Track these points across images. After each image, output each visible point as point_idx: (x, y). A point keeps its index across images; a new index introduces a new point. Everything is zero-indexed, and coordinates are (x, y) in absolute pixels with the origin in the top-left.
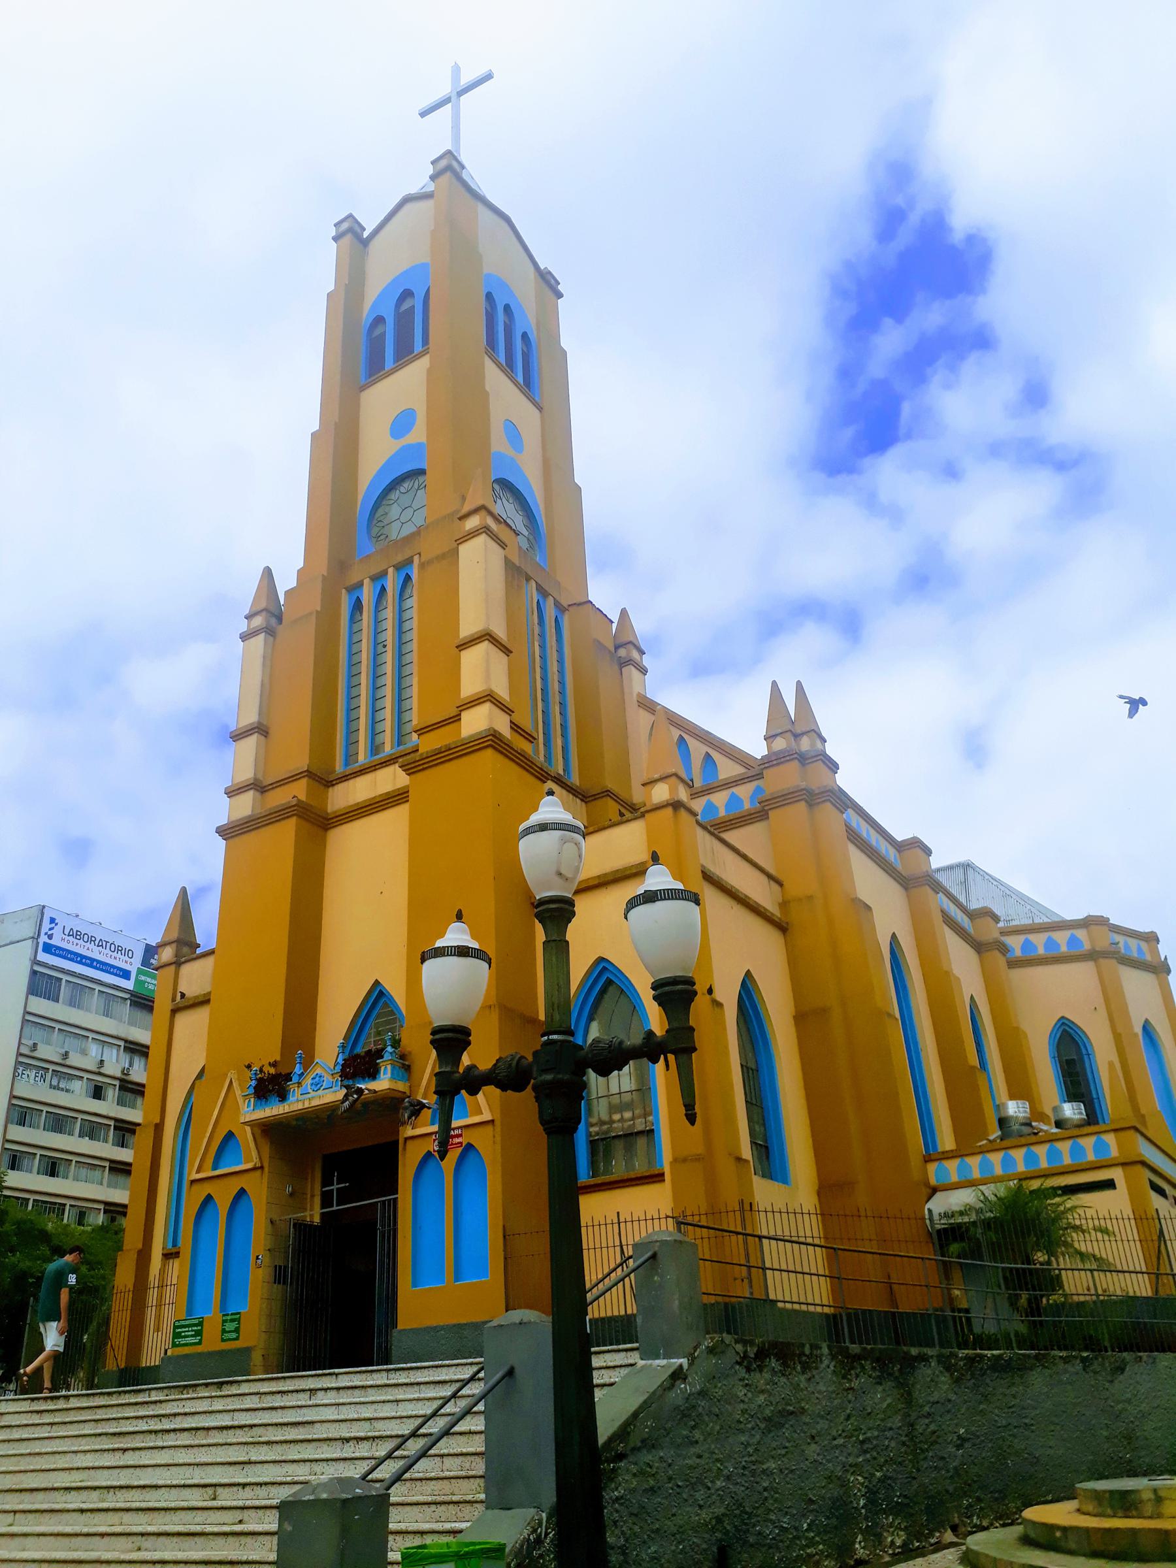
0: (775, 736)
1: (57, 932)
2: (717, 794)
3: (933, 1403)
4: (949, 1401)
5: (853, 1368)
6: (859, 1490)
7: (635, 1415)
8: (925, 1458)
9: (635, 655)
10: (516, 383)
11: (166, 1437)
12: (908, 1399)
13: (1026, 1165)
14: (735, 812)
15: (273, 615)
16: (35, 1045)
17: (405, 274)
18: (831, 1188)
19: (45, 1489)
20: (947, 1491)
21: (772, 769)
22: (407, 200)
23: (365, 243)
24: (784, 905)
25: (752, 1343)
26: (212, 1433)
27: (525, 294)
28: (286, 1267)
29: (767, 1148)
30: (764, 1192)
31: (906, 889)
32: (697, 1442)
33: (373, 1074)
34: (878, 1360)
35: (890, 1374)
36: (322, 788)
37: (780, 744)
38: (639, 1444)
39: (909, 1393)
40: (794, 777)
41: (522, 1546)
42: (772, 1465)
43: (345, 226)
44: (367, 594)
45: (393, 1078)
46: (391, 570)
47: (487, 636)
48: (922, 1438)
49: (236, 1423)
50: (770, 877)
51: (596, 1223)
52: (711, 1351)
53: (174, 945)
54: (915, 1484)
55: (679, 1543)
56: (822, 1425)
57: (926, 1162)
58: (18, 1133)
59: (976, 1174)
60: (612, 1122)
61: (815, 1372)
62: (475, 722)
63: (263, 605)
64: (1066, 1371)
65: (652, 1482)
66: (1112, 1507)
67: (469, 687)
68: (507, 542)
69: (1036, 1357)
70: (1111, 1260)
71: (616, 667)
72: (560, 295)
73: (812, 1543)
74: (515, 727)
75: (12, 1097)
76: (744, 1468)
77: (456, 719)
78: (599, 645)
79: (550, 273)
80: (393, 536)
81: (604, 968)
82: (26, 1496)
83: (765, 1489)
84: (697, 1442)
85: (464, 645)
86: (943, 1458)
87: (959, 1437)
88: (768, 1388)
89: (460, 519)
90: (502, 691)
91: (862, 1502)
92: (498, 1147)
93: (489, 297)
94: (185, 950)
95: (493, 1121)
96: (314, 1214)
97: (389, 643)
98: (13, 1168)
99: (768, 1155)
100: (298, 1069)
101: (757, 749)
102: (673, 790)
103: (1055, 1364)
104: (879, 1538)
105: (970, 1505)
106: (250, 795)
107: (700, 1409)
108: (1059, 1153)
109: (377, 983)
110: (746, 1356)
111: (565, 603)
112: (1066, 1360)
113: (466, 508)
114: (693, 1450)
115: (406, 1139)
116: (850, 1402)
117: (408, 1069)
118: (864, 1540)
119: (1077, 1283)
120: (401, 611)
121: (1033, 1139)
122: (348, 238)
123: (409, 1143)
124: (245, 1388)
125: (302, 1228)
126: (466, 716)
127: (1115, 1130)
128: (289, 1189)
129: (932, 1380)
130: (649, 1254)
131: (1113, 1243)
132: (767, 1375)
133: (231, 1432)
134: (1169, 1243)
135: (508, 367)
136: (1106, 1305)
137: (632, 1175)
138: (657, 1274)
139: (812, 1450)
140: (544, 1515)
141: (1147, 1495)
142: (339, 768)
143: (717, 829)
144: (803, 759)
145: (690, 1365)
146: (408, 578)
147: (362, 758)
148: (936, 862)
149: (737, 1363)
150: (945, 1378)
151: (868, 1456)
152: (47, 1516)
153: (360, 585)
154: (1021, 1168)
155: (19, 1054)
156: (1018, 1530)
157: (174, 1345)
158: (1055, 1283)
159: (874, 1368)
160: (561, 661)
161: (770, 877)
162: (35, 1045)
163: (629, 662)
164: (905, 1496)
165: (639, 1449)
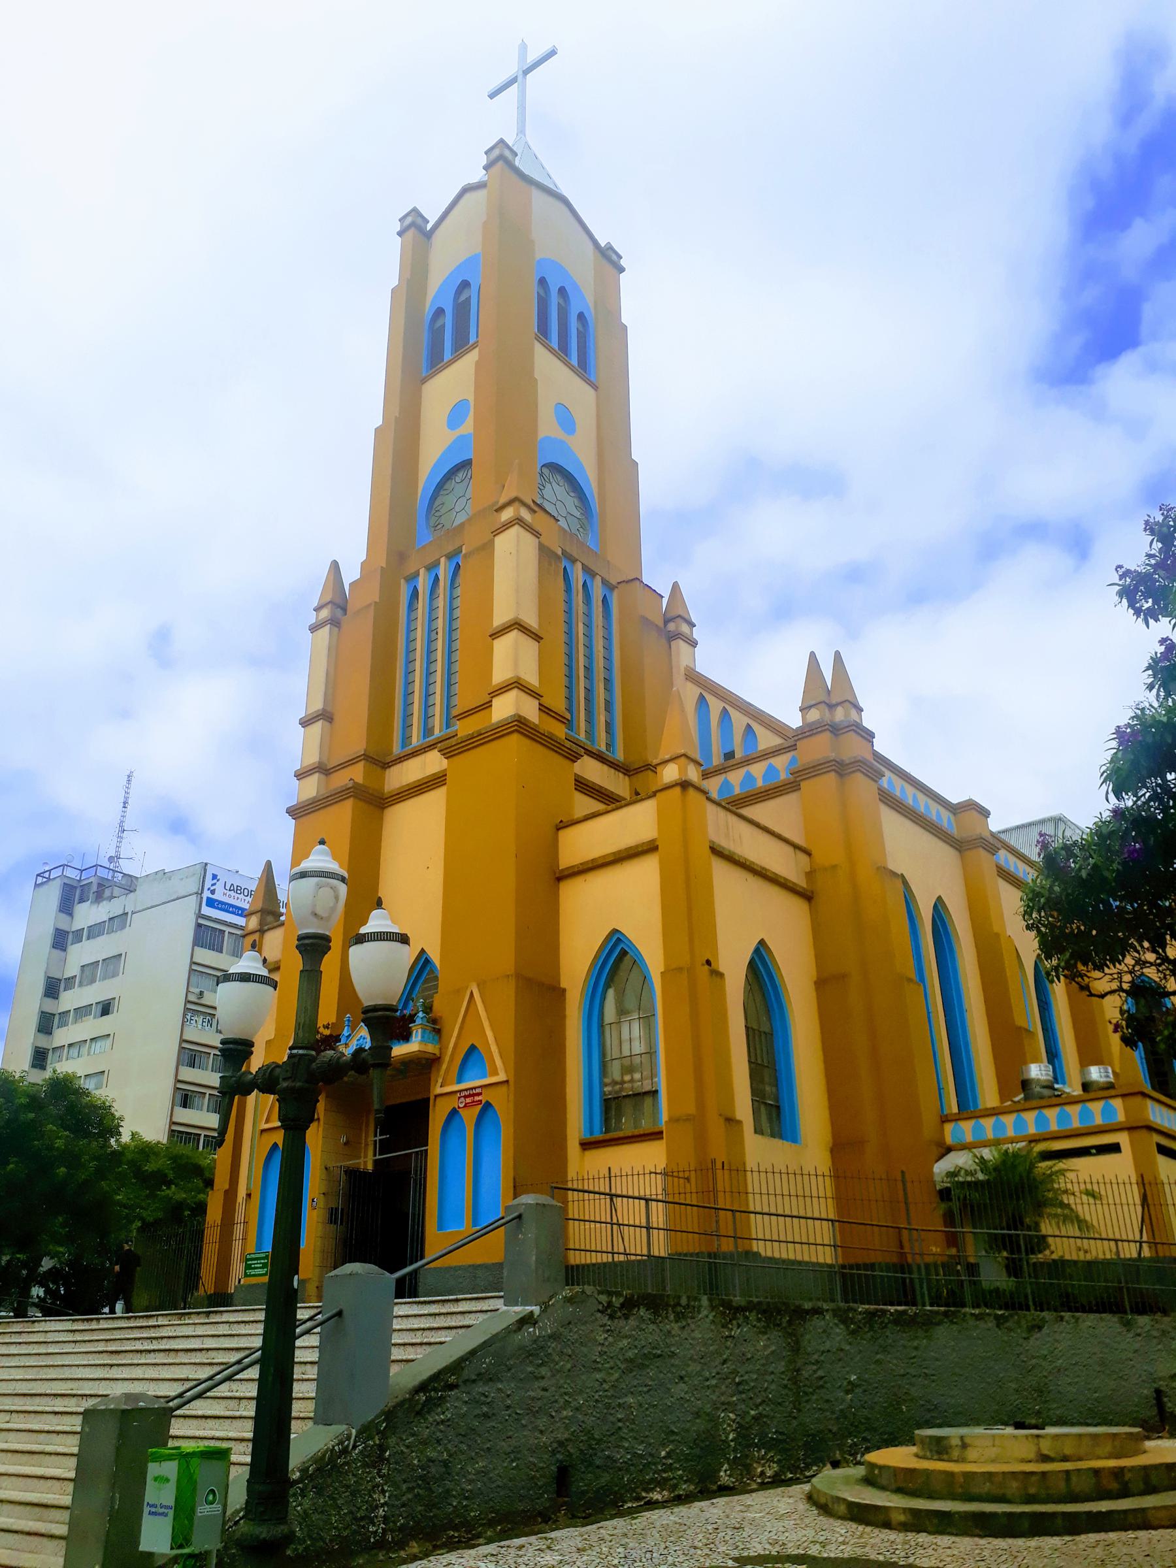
0: (810, 707)
1: (219, 888)
2: (755, 765)
3: (823, 1352)
4: (842, 1350)
5: (734, 1319)
6: (729, 1425)
7: (473, 1353)
8: (807, 1401)
9: (685, 628)
10: (567, 364)
11: (148, 1355)
12: (796, 1349)
13: (1059, 1123)
14: (773, 782)
15: (339, 607)
16: (201, 993)
17: (458, 268)
18: (843, 1146)
19: (40, 1395)
20: (830, 1431)
21: (805, 740)
22: (466, 190)
23: (429, 235)
24: (810, 875)
25: (618, 1294)
26: (180, 1354)
27: (582, 272)
28: (337, 1209)
29: (778, 1107)
30: (759, 1150)
31: (960, 851)
32: (543, 1378)
33: (406, 1037)
34: (764, 1312)
35: (778, 1325)
36: (379, 769)
37: (814, 715)
38: (474, 1377)
39: (797, 1342)
40: (830, 746)
41: (324, 1455)
42: (630, 1400)
43: (409, 220)
44: (423, 583)
45: (423, 1041)
46: (443, 560)
47: (517, 625)
48: (808, 1383)
49: (205, 1346)
50: (796, 847)
51: (635, 1172)
52: (569, 1300)
53: (259, 915)
54: (795, 1423)
55: (513, 1461)
56: (694, 1367)
57: (943, 1122)
58: (188, 1074)
59: (969, 1138)
60: (623, 1082)
61: (689, 1321)
62: (503, 708)
63: (328, 598)
64: (976, 1327)
65: (485, 1409)
66: (931, 1451)
67: (500, 675)
68: (540, 531)
69: (946, 1314)
70: (1095, 1223)
71: (664, 641)
72: (622, 270)
73: (670, 1468)
74: (544, 709)
75: (183, 1041)
76: (597, 1401)
77: (487, 705)
78: (646, 621)
79: (611, 248)
80: (448, 526)
81: (619, 940)
82: (28, 1400)
83: (619, 1420)
84: (543, 1378)
85: (495, 635)
86: (828, 1401)
87: (850, 1382)
88: (640, 1332)
89: (496, 511)
90: (531, 677)
91: (731, 1437)
92: (511, 1105)
93: (542, 282)
94: (270, 918)
95: (507, 1081)
96: (367, 1161)
97: (440, 631)
98: (185, 1106)
99: (774, 1114)
100: (346, 1032)
101: (794, 721)
102: (682, 770)
103: (963, 1320)
104: (748, 1468)
105: (855, 1444)
106: (315, 778)
107: (550, 1351)
108: (1004, 1126)
109: (423, 951)
110: (610, 1304)
111: (614, 582)
112: (978, 1317)
113: (502, 501)
114: (537, 1384)
115: (436, 1096)
116: (727, 1348)
117: (438, 1032)
118: (731, 1469)
119: (1063, 1244)
120: (452, 599)
121: (1055, 1101)
122: (410, 234)
123: (438, 1099)
124: (225, 1317)
125: (353, 1175)
126: (496, 702)
127: (1123, 1096)
128: (343, 1139)
129: (824, 1331)
130: (516, 1214)
131: (1099, 1207)
132: (632, 1322)
133: (194, 1354)
134: (1152, 1208)
135: (562, 351)
136: (1091, 1267)
137: (636, 1132)
138: (521, 1233)
139: (679, 1390)
140: (354, 1431)
141: (955, 1442)
142: (397, 750)
143: (734, 805)
144: (835, 730)
145: (543, 1311)
146: (437, 579)
147: (416, 741)
148: (995, 824)
149: (599, 1311)
150: (840, 1330)
151: (744, 1396)
152: (32, 1415)
153: (417, 574)
154: (1032, 1130)
155: (187, 1002)
156: (861, 1471)
157: (246, 1275)
158: (1041, 1243)
159: (759, 1320)
160: (608, 638)
161: (796, 847)
162: (201, 993)
163: (678, 636)
164: (782, 1433)
165: (474, 1381)
